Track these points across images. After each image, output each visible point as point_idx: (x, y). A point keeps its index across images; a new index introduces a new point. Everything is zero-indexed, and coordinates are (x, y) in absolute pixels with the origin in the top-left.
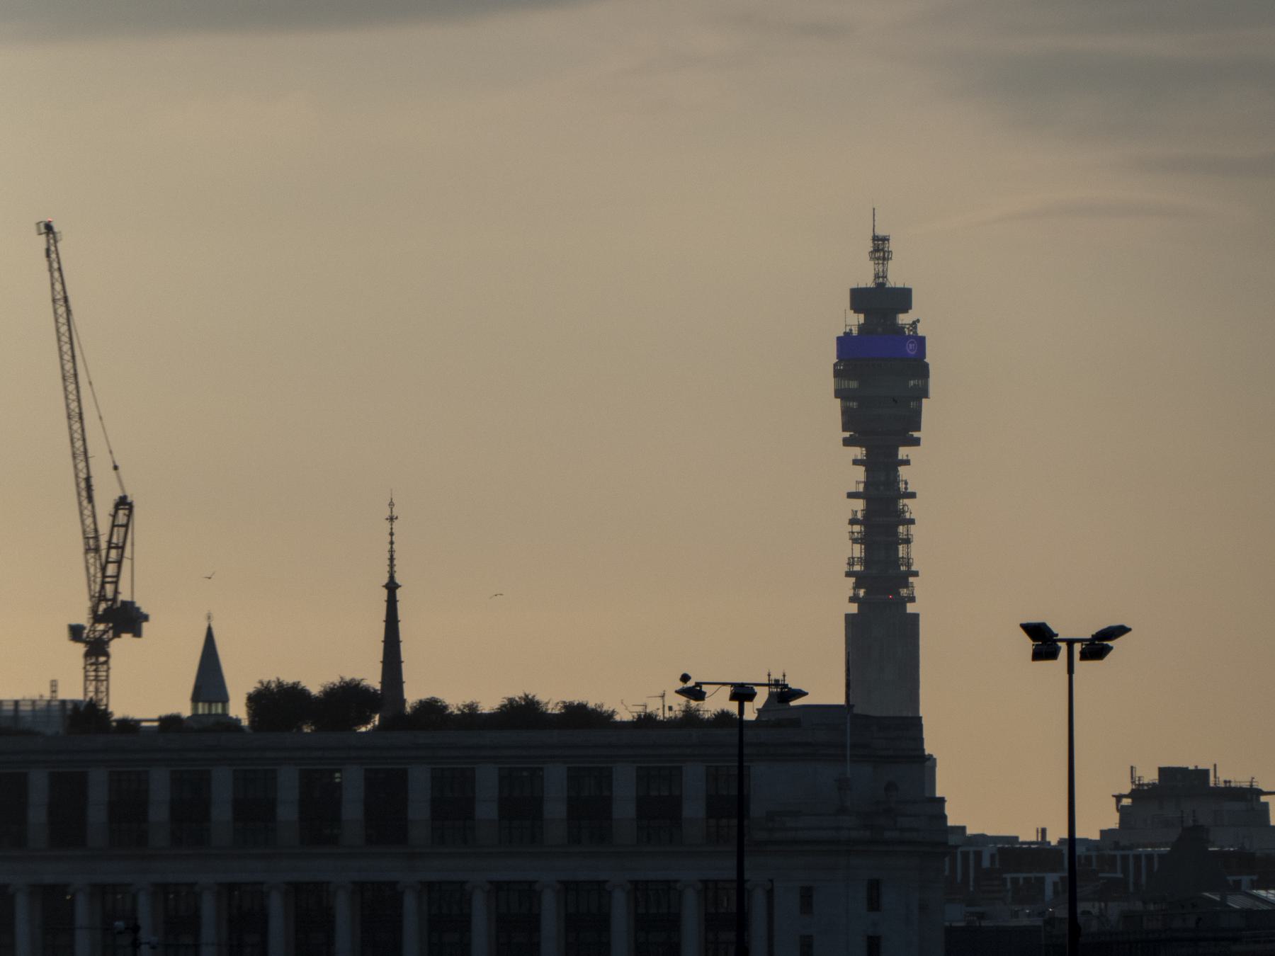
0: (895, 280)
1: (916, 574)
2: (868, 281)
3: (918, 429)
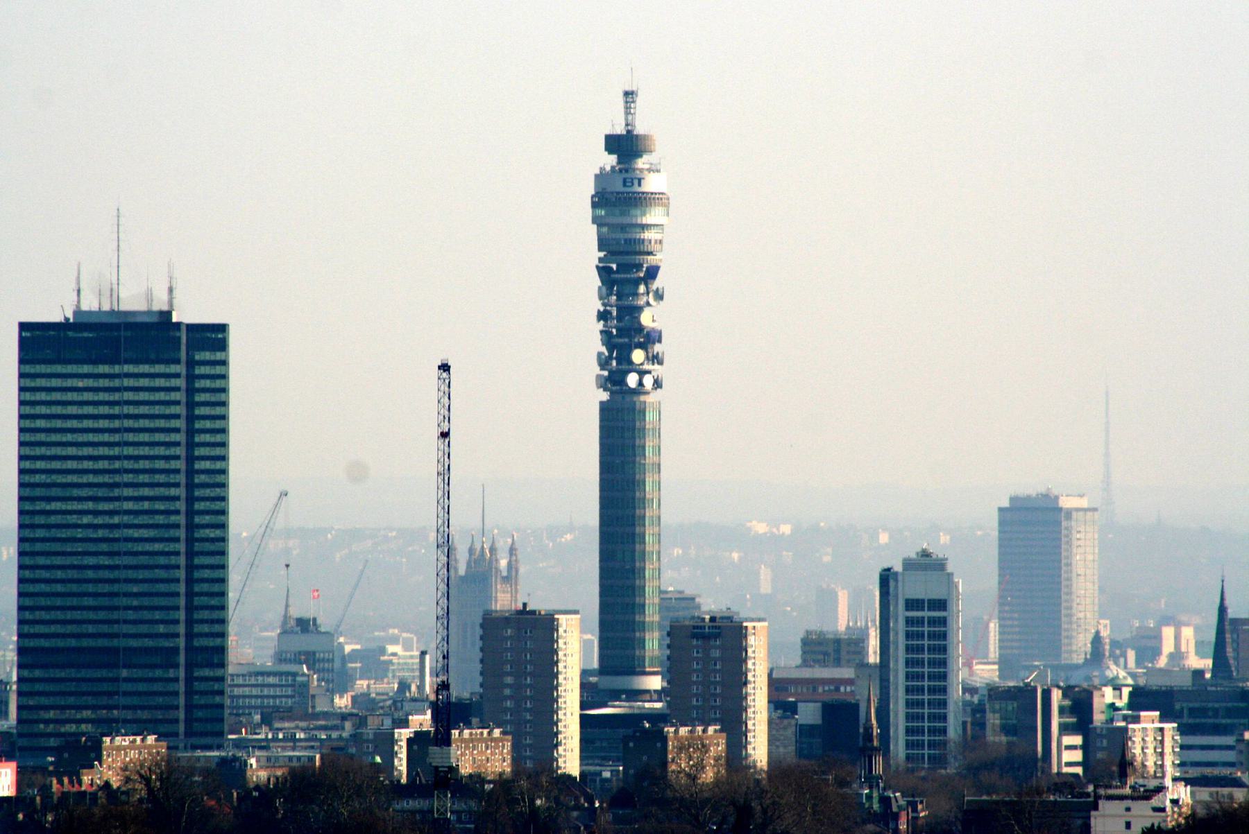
0: (639, 129)
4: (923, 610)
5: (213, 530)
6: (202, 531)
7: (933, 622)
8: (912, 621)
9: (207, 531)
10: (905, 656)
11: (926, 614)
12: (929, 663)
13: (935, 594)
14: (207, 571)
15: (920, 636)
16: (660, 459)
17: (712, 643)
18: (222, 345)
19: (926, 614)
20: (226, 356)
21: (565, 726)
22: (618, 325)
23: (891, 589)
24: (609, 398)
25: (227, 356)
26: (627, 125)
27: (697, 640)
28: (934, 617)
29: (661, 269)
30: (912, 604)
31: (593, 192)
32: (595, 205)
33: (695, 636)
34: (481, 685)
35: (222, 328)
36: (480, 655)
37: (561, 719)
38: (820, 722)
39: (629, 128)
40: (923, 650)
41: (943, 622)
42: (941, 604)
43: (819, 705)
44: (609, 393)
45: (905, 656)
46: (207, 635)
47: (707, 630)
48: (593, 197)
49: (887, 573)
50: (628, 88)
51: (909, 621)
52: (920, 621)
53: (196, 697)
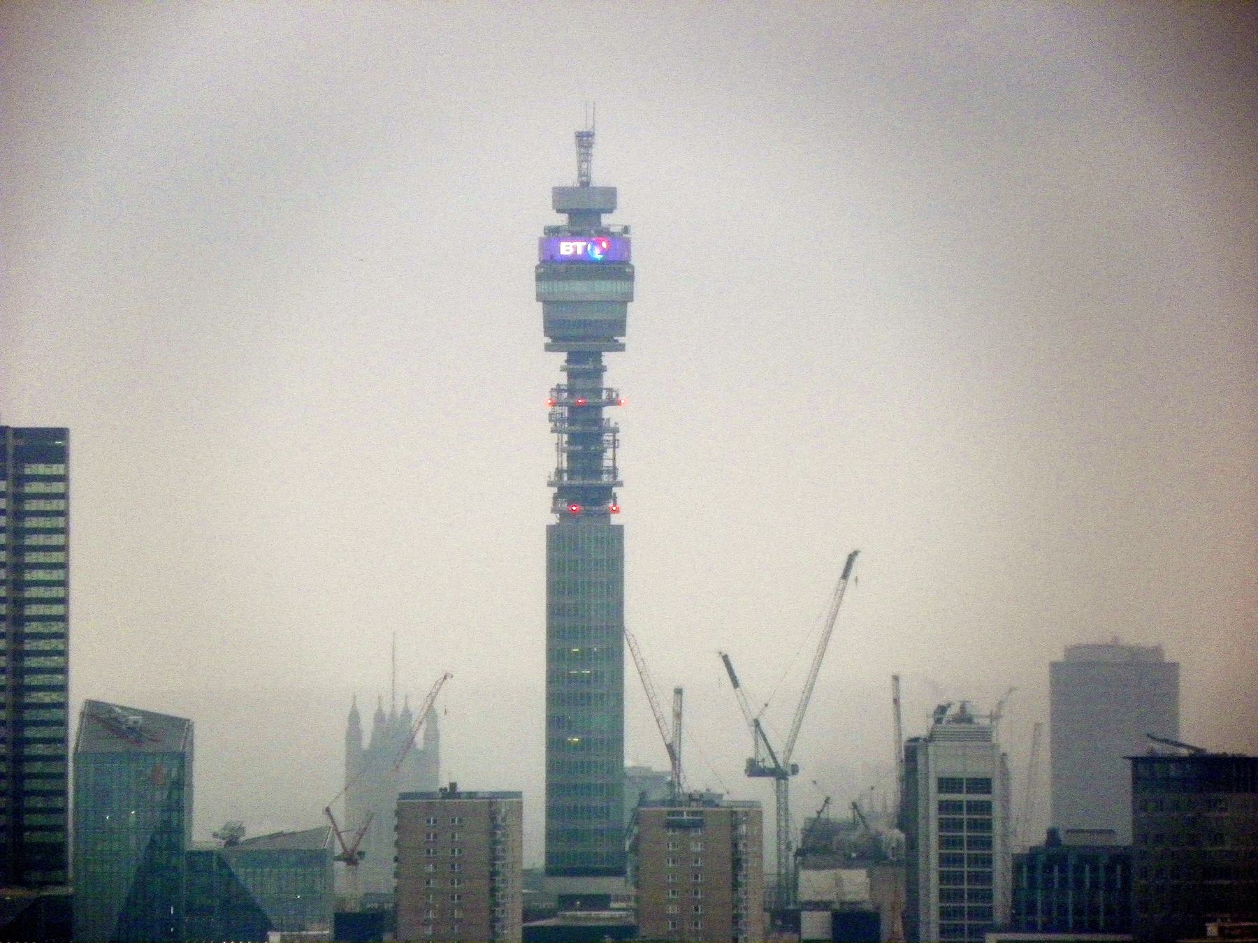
0: (599, 179)
1: (620, 484)
2: (570, 179)
3: (623, 335)
4: (960, 792)
5: (48, 693)
6: (34, 694)
7: (973, 807)
8: (948, 860)
9: (40, 694)
10: (939, 905)
11: (963, 797)
12: (970, 896)
13: (976, 769)
14: (40, 745)
15: (958, 825)
16: (618, 225)
17: (693, 834)
18: (61, 456)
19: (963, 797)
20: (65, 715)
21: (503, 835)
22: (570, 428)
23: (920, 767)
24: (558, 521)
25: (67, 698)
26: (580, 175)
27: (674, 831)
28: (975, 802)
29: (620, 193)
30: (947, 784)
31: (537, 262)
32: (539, 278)
33: (670, 825)
34: (397, 875)
35: (62, 433)
36: (394, 852)
37: (499, 872)
38: (828, 937)
39: (584, 179)
40: (961, 860)
41: (986, 807)
42: (983, 785)
43: (827, 914)
44: (558, 515)
45: (940, 922)
46: (41, 828)
47: (685, 817)
48: (537, 268)
49: (913, 744)
50: (582, 129)
51: (944, 807)
52: (957, 806)
53: (27, 833)
